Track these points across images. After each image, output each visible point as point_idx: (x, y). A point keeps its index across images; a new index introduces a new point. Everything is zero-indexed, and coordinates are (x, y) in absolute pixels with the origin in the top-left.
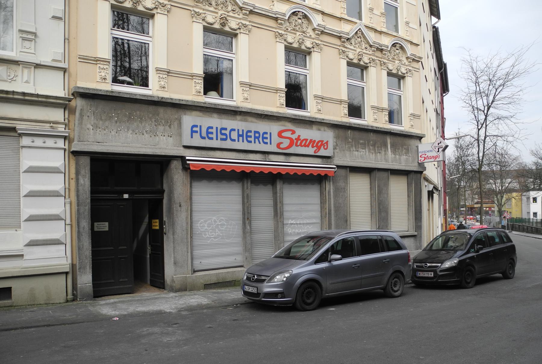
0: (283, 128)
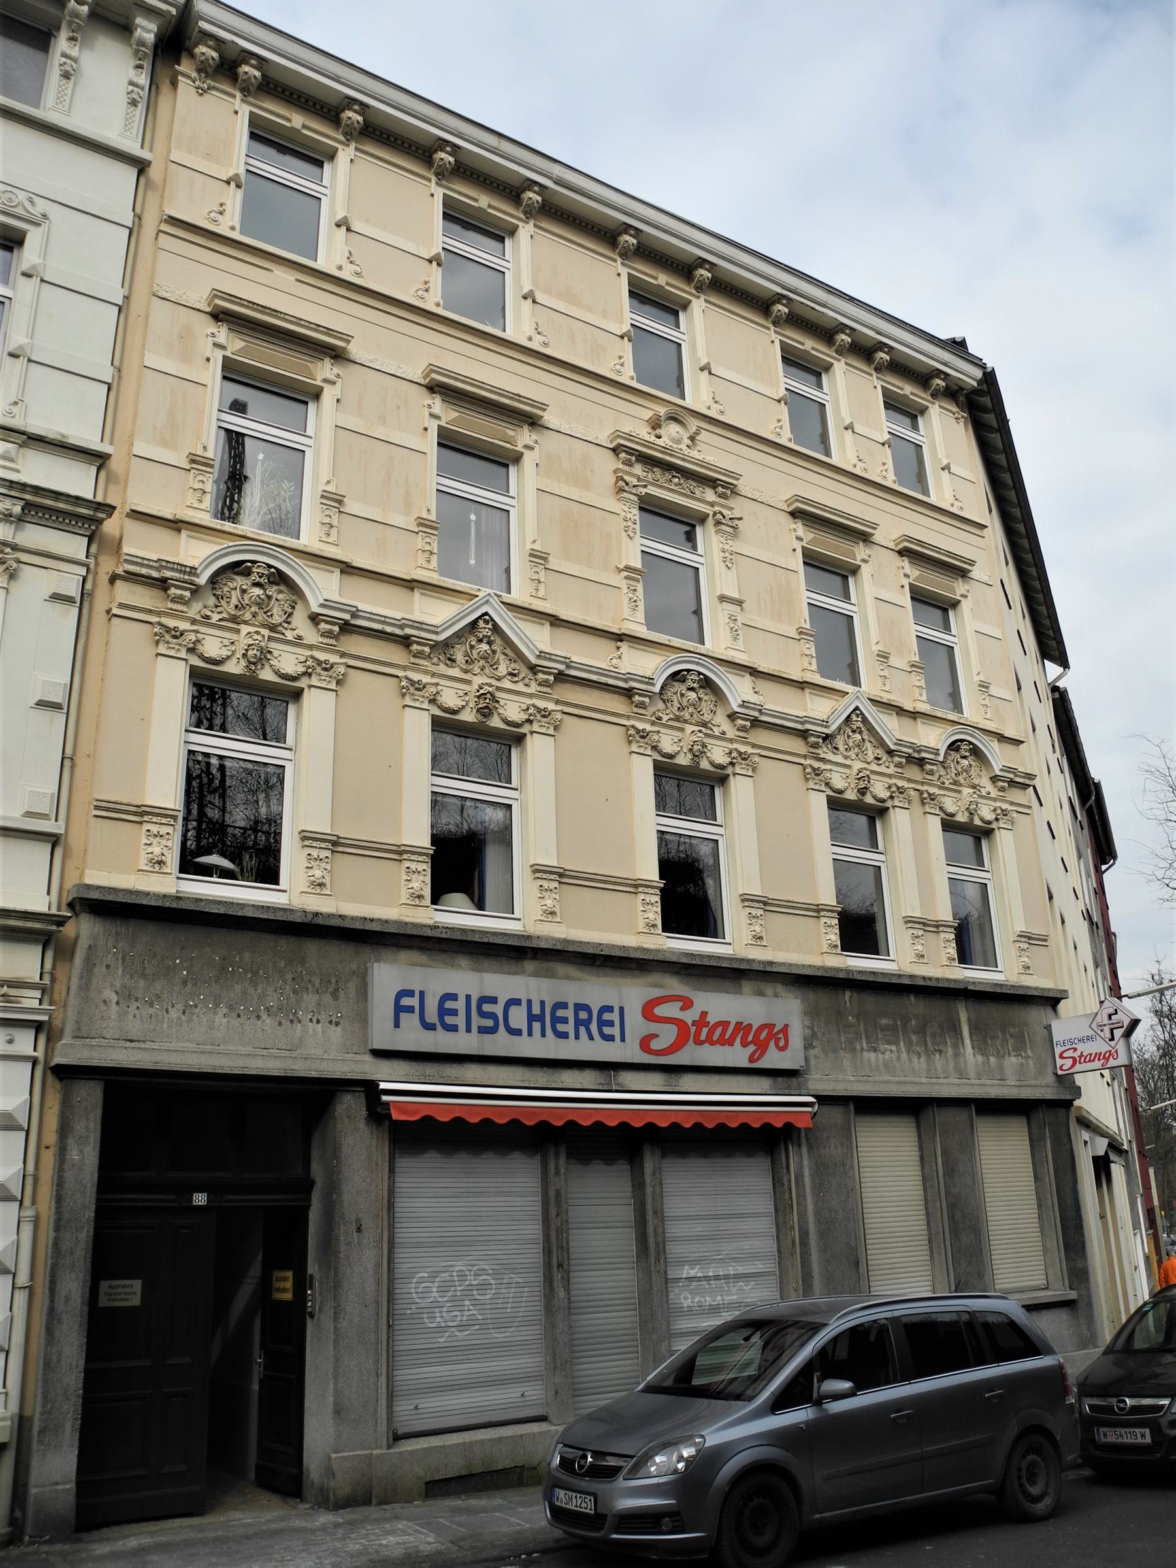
0: (657, 993)
